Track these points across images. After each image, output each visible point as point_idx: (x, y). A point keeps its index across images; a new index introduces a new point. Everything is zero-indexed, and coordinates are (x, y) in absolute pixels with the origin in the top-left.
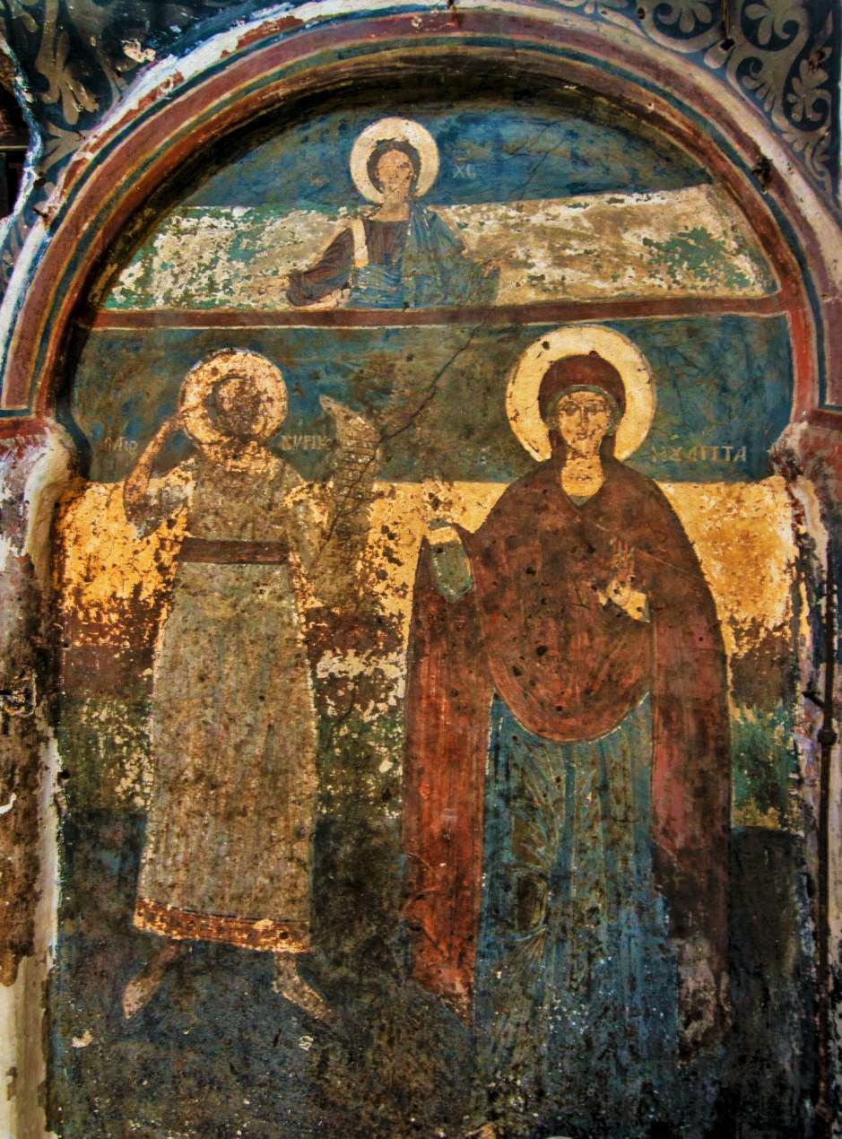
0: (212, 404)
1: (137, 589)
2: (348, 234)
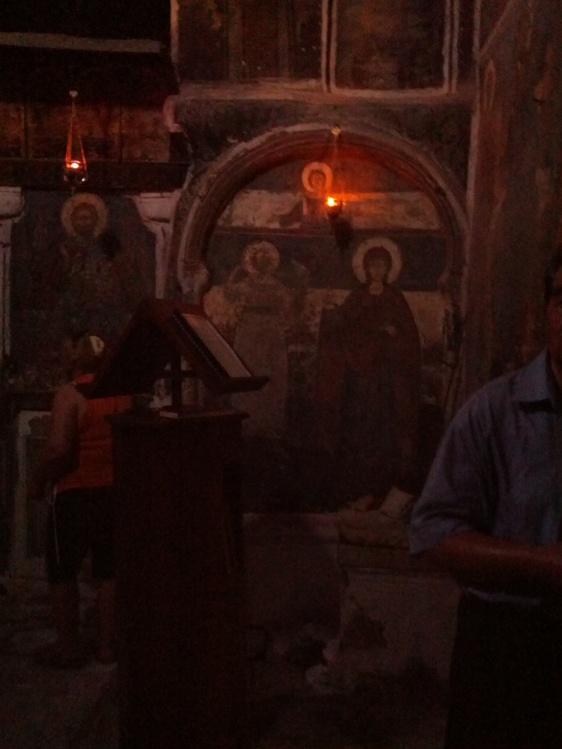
0: (254, 259)
1: (228, 323)
2: (301, 202)
